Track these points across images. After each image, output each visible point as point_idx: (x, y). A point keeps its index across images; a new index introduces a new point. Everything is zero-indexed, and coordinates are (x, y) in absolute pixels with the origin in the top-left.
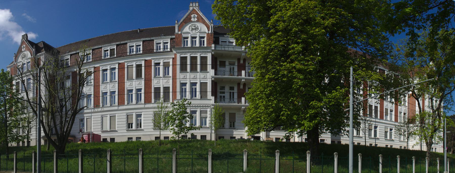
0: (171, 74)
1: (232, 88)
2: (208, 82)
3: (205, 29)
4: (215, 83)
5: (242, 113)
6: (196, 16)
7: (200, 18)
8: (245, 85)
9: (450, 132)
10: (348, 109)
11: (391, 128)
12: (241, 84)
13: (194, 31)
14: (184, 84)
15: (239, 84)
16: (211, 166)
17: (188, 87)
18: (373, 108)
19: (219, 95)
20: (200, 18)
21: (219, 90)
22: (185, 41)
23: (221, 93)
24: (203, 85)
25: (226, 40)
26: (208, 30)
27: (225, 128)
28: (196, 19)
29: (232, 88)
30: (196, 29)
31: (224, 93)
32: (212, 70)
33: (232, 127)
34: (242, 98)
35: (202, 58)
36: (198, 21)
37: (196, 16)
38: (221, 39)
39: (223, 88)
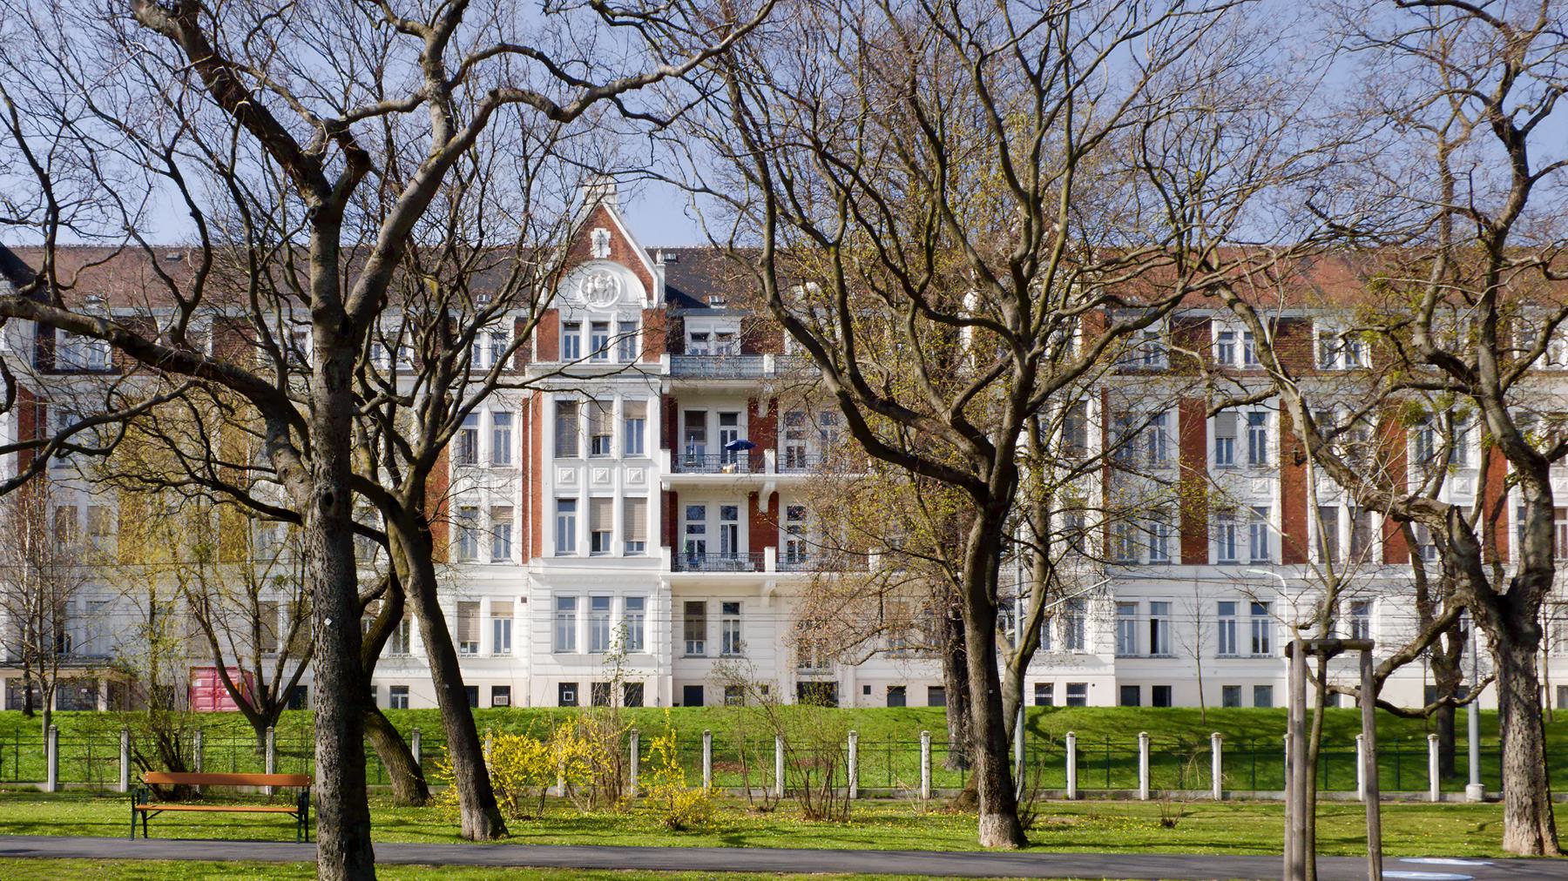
0: (516, 461)
1: (730, 513)
2: (648, 495)
3: (636, 289)
4: (670, 499)
5: (766, 600)
6: (608, 235)
7: (620, 247)
8: (774, 498)
9: (1445, 650)
10: (1323, 751)
11: (561, 397)
12: (761, 496)
13: (600, 304)
14: (566, 504)
15: (754, 498)
16: (979, 666)
17: (581, 514)
18: (1259, 531)
19: (684, 538)
20: (620, 247)
21: (683, 523)
22: (568, 338)
23: (691, 530)
24: (632, 505)
25: (709, 326)
26: (650, 297)
27: (705, 657)
28: (607, 251)
29: (730, 513)
30: (607, 292)
31: (702, 530)
32: (661, 452)
33: (695, 653)
34: (766, 549)
35: (628, 405)
36: (613, 257)
37: (608, 235)
38: (692, 326)
39: (699, 512)
